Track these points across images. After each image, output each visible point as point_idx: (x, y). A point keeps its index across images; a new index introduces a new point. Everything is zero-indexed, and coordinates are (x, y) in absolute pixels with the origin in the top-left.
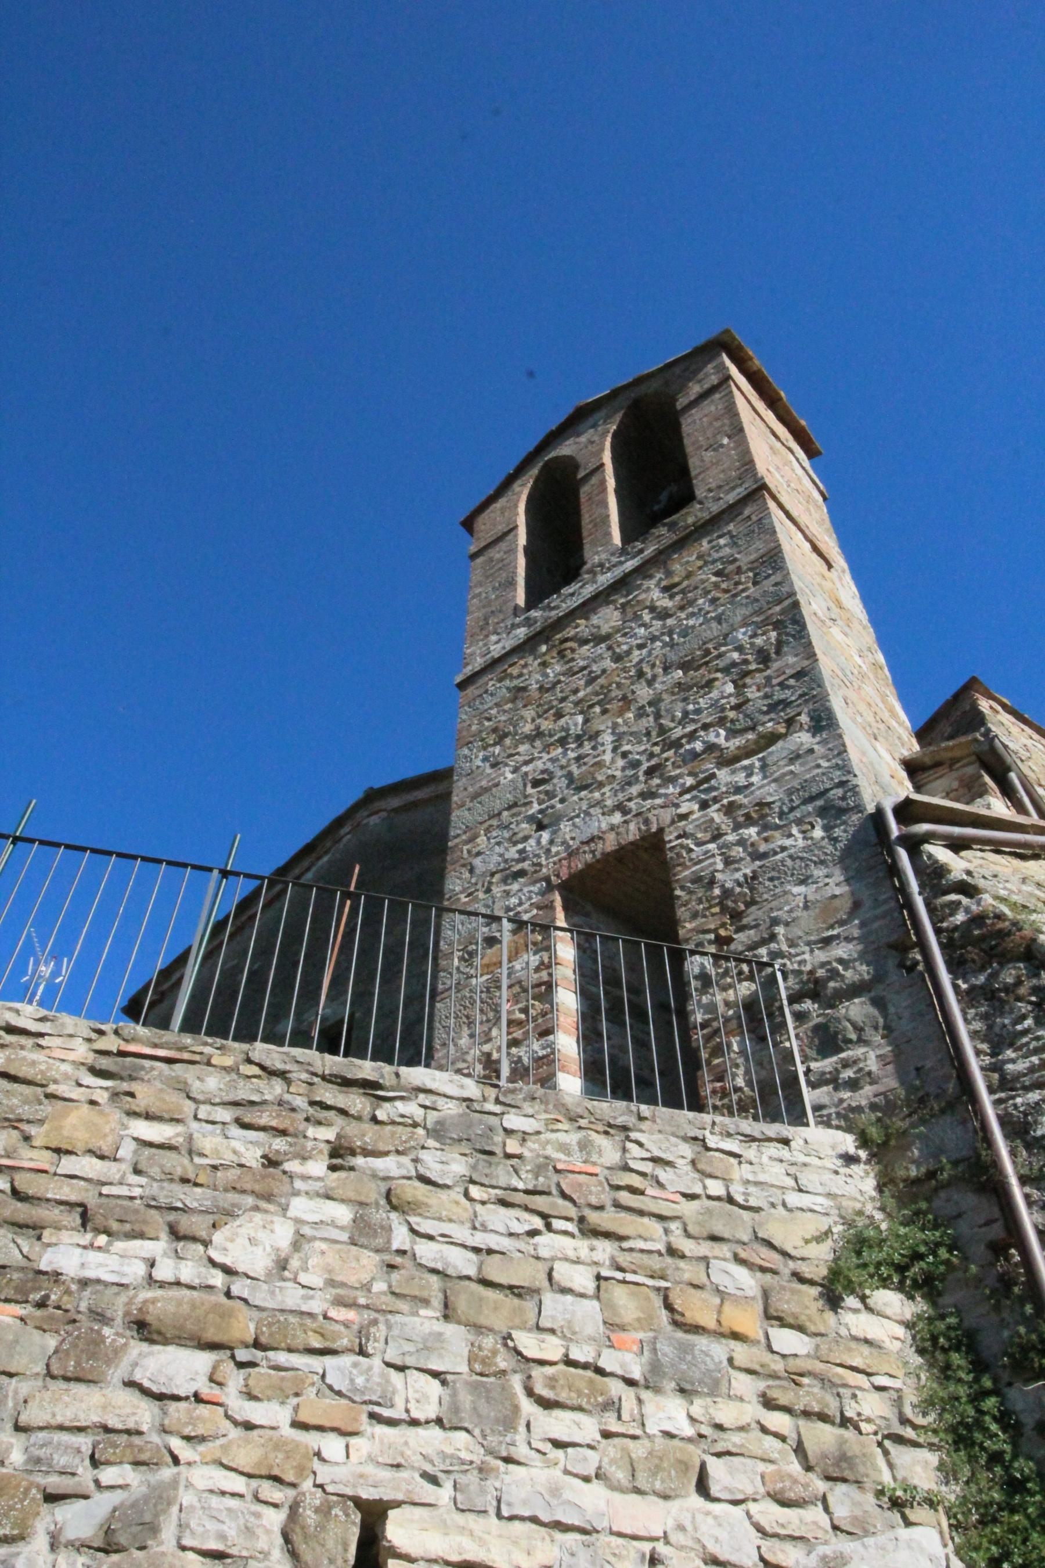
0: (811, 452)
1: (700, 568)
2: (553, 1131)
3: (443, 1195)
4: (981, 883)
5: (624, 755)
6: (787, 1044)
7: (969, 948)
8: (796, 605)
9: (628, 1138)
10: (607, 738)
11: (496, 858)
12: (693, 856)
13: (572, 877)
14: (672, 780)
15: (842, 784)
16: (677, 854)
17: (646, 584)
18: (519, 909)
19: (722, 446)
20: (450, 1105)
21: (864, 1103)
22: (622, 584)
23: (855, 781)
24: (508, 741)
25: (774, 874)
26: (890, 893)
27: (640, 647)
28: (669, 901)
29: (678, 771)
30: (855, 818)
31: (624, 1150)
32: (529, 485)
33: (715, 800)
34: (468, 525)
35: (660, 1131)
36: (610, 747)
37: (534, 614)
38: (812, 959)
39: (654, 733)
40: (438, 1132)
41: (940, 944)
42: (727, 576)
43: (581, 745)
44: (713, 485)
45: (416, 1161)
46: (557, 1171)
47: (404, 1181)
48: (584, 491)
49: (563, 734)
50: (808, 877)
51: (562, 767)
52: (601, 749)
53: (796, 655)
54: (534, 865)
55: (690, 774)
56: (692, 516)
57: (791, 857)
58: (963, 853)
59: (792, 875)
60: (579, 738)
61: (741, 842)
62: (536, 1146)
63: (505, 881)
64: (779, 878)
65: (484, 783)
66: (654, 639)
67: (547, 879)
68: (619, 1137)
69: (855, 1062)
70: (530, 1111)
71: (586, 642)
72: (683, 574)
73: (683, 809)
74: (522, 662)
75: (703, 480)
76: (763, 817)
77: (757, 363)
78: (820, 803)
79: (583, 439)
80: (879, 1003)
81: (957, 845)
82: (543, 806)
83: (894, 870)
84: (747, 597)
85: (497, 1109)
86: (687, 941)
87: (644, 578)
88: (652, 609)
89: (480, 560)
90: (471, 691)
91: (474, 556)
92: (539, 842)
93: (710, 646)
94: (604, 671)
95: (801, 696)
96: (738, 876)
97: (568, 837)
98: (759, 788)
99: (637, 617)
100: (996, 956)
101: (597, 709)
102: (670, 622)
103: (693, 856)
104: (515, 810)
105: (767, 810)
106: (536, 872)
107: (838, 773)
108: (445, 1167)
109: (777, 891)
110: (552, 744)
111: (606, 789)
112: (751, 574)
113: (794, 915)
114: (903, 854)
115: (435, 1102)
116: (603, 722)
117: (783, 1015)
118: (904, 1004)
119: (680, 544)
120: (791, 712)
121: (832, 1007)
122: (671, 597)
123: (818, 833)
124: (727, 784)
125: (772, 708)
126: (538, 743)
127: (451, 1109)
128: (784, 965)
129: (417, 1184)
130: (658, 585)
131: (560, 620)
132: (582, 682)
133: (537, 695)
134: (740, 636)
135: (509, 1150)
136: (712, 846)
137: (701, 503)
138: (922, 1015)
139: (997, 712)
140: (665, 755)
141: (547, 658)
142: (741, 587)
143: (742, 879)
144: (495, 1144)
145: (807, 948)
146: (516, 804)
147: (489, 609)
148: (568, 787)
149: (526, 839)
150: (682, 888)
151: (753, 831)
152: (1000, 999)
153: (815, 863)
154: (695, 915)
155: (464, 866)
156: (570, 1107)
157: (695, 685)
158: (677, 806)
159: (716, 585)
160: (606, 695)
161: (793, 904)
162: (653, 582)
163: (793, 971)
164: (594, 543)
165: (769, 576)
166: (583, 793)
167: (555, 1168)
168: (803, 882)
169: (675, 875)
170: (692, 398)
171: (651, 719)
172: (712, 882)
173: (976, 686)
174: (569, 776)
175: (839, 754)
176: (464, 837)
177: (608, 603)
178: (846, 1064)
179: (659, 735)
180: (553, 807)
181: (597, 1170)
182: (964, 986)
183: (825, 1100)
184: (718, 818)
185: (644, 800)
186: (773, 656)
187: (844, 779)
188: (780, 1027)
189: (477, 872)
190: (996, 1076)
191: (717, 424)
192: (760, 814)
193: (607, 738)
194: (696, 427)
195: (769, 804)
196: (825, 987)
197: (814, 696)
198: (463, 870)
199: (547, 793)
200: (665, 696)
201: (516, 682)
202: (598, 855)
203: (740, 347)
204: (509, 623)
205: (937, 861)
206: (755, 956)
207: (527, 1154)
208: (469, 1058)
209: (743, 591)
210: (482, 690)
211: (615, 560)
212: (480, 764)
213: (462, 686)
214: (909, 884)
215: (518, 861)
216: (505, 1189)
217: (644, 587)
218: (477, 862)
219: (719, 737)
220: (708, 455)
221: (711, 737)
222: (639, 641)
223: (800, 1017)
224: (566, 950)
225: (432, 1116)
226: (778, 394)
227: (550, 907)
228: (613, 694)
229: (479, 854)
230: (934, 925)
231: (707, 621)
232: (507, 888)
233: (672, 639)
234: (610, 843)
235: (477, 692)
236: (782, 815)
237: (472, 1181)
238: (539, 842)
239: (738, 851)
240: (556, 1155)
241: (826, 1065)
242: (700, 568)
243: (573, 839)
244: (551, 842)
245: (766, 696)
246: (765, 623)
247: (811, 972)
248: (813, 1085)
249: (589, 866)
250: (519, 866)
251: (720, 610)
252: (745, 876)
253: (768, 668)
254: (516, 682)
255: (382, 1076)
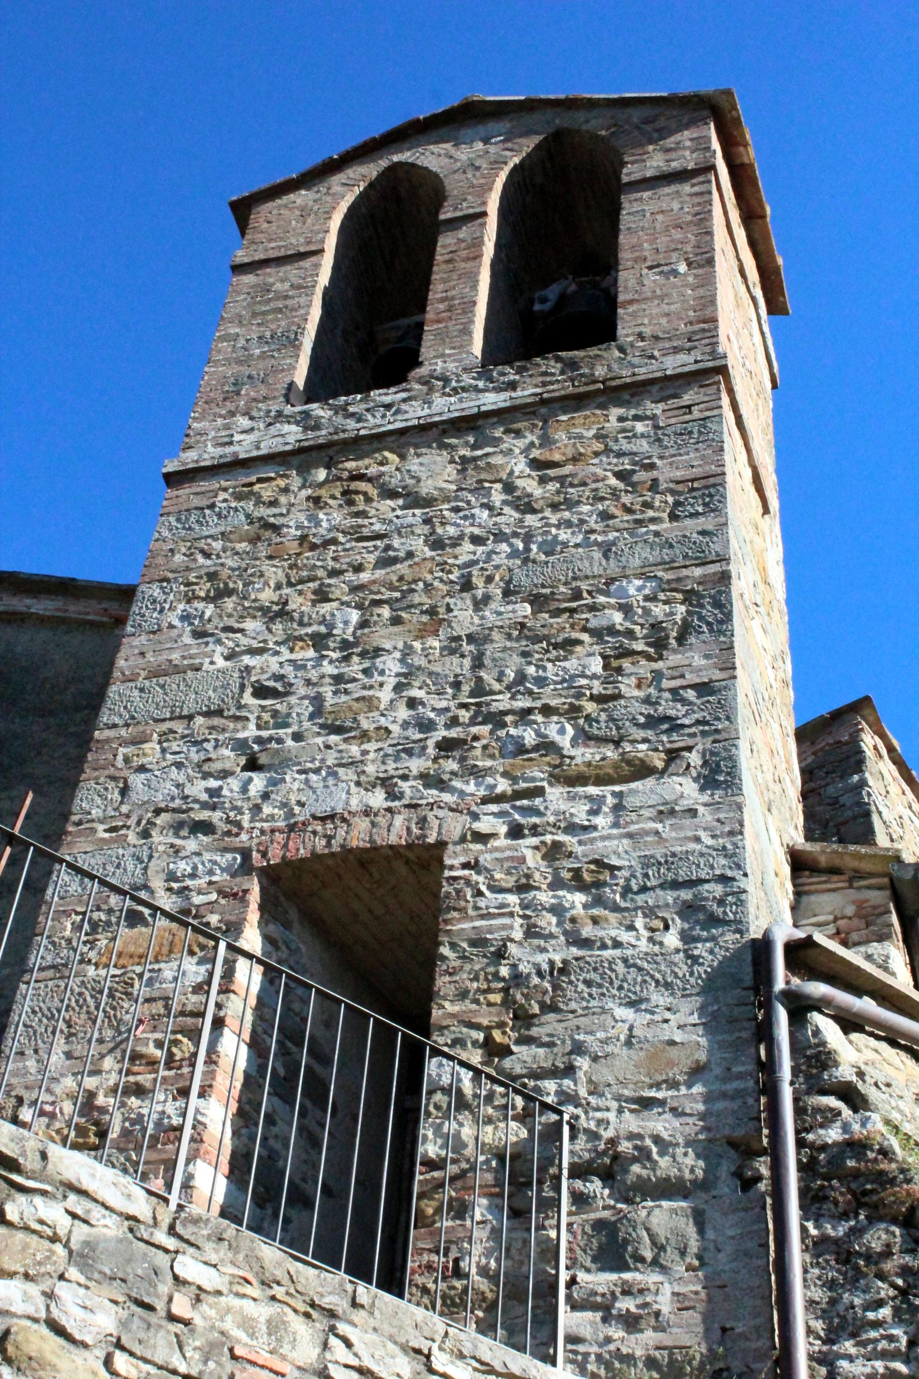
0: (775, 305)
1: (596, 454)
2: (237, 1294)
3: (78, 1355)
4: (872, 1094)
5: (412, 703)
6: (553, 1234)
7: (835, 1182)
8: (725, 578)
9: (332, 1329)
10: (391, 665)
11: (168, 787)
12: (482, 903)
13: (286, 863)
14: (476, 773)
15: (724, 879)
16: (458, 892)
17: (509, 441)
18: (189, 882)
19: (675, 273)
20: (108, 1221)
21: (639, 1353)
22: (469, 424)
23: (743, 883)
24: (229, 603)
25: (593, 976)
26: (751, 1067)
27: (477, 540)
28: (429, 961)
29: (489, 763)
30: (730, 938)
31: (325, 1346)
32: (357, 191)
33: (535, 830)
34: (242, 210)
35: (375, 1329)
36: (392, 682)
37: (317, 409)
38: (620, 1124)
39: (466, 688)
40: (83, 1257)
41: (799, 1161)
42: (634, 485)
43: (346, 659)
44: (647, 331)
45: (49, 1295)
46: (234, 1357)
47: (28, 1323)
48: (446, 242)
49: (323, 629)
50: (641, 1001)
51: (308, 682)
52: (377, 678)
53: (707, 657)
54: (228, 821)
55: (505, 774)
56: (604, 364)
57: (625, 960)
58: (855, 1036)
59: (620, 988)
60: (345, 645)
61: (557, 910)
62: (212, 1313)
63: (177, 828)
64: (600, 986)
65: (175, 656)
66: (500, 537)
67: (246, 854)
68: (322, 1323)
69: (641, 1291)
70: (213, 1258)
71: (392, 494)
72: (570, 452)
73: (484, 825)
74: (282, 483)
75: (634, 315)
76: (598, 884)
77: (751, 154)
78: (686, 895)
79: (464, 154)
80: (700, 1219)
81: (850, 1023)
82: (265, 734)
83: (764, 1032)
84: (657, 534)
85: (171, 1243)
86: (442, 1029)
87: (507, 431)
88: (509, 488)
89: (248, 279)
90: (186, 494)
91: (239, 269)
92: (244, 789)
93: (584, 586)
94: (410, 555)
95: (698, 722)
96: (541, 959)
97: (293, 798)
98: (603, 838)
99: (479, 489)
100: (866, 1205)
101: (386, 612)
102: (531, 520)
103: (482, 903)
104: (216, 721)
105: (606, 876)
106: (228, 833)
107: (723, 861)
108: (87, 1316)
109: (593, 1003)
110: (300, 638)
111: (371, 746)
112: (670, 499)
113: (609, 1049)
114: (782, 1015)
115: (88, 1211)
116: (389, 637)
117: (558, 1189)
118: (730, 1233)
119: (576, 402)
120: (678, 740)
121: (629, 1201)
122: (543, 481)
123: (672, 940)
124: (556, 813)
125: (652, 722)
126: (278, 627)
127: (109, 1228)
128: (577, 1118)
129: (44, 1330)
130: (526, 451)
131: (358, 440)
132: (372, 558)
133: (294, 547)
134: (632, 591)
135: (176, 1310)
136: (512, 899)
137: (622, 350)
138: (746, 1254)
139: (881, 757)
140: (475, 730)
141: (323, 492)
142: (650, 513)
143: (545, 967)
144: (158, 1297)
145: (614, 1105)
146: (219, 713)
147: (246, 371)
148: (312, 717)
149: (225, 774)
150: (453, 946)
151: (579, 898)
152: (857, 1268)
153: (657, 982)
154: (463, 995)
155: (113, 778)
156: (267, 1264)
157: (546, 638)
158: (475, 817)
159: (615, 494)
160: (404, 594)
161: (612, 1033)
162: (521, 443)
163: (587, 1131)
164: (442, 337)
165: (697, 514)
166: (333, 739)
167: (231, 1350)
168: (632, 1004)
169: (446, 922)
170: (649, 174)
171: (467, 662)
172: (500, 955)
173: (866, 712)
174: (318, 700)
175: (731, 833)
176: (123, 732)
177: (442, 446)
178: (627, 1291)
179: (472, 695)
180: (280, 741)
181: (286, 1368)
182: (814, 1232)
183: (586, 1332)
184: (533, 860)
185: (427, 786)
186: (673, 641)
187: (729, 873)
188: (551, 1205)
189: (133, 796)
190: (823, 1371)
191: (677, 235)
192: (593, 879)
193: (391, 665)
194: (645, 223)
195: (613, 868)
196: (626, 1171)
197: (717, 731)
198: (111, 785)
199: (275, 714)
200: (496, 635)
201: (264, 512)
202: (336, 848)
203: (737, 121)
204: (274, 408)
205: (823, 1044)
206: (537, 1089)
207: (198, 1321)
208: (58, 1089)
209: (653, 520)
210: (205, 502)
211: (467, 380)
212: (176, 622)
213: (173, 479)
214: (780, 1065)
215: (205, 806)
216: (160, 1368)
217: (504, 446)
218: (137, 781)
219: (562, 734)
220: (652, 278)
221: (552, 732)
222: (476, 531)
223: (580, 1200)
224: (249, 978)
225: (80, 1232)
226: (763, 209)
227: (241, 897)
228: (416, 599)
229: (142, 769)
230: (798, 1132)
231: (586, 544)
232: (178, 842)
233: (527, 550)
234: (358, 835)
235: (197, 502)
236: (626, 891)
237: (119, 1345)
238: (244, 789)
239: (548, 922)
240: (239, 1334)
241: (600, 1281)
242: (596, 454)
243: (301, 804)
244: (266, 796)
245: (647, 701)
246: (672, 586)
247: (613, 1142)
248: (575, 1306)
249: (315, 856)
250: (204, 815)
251: (612, 536)
252: (551, 963)
253: (661, 658)
254: (264, 512)
255: (24, 1153)
